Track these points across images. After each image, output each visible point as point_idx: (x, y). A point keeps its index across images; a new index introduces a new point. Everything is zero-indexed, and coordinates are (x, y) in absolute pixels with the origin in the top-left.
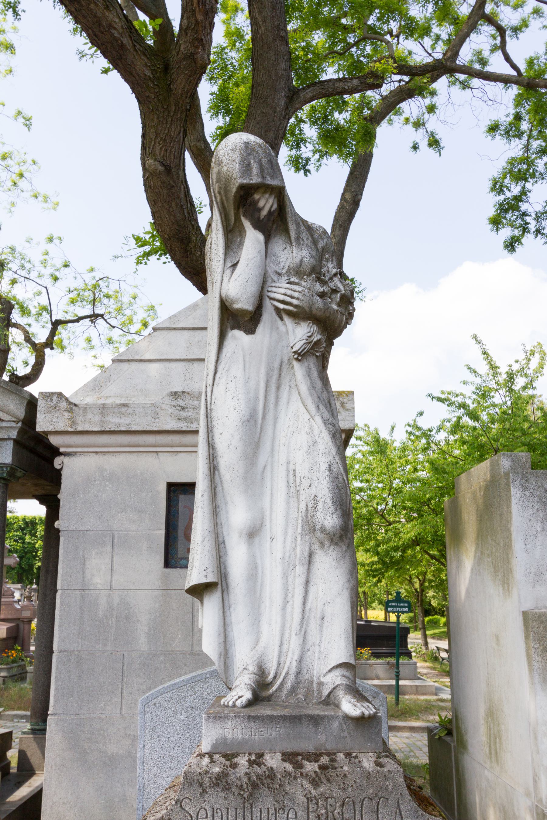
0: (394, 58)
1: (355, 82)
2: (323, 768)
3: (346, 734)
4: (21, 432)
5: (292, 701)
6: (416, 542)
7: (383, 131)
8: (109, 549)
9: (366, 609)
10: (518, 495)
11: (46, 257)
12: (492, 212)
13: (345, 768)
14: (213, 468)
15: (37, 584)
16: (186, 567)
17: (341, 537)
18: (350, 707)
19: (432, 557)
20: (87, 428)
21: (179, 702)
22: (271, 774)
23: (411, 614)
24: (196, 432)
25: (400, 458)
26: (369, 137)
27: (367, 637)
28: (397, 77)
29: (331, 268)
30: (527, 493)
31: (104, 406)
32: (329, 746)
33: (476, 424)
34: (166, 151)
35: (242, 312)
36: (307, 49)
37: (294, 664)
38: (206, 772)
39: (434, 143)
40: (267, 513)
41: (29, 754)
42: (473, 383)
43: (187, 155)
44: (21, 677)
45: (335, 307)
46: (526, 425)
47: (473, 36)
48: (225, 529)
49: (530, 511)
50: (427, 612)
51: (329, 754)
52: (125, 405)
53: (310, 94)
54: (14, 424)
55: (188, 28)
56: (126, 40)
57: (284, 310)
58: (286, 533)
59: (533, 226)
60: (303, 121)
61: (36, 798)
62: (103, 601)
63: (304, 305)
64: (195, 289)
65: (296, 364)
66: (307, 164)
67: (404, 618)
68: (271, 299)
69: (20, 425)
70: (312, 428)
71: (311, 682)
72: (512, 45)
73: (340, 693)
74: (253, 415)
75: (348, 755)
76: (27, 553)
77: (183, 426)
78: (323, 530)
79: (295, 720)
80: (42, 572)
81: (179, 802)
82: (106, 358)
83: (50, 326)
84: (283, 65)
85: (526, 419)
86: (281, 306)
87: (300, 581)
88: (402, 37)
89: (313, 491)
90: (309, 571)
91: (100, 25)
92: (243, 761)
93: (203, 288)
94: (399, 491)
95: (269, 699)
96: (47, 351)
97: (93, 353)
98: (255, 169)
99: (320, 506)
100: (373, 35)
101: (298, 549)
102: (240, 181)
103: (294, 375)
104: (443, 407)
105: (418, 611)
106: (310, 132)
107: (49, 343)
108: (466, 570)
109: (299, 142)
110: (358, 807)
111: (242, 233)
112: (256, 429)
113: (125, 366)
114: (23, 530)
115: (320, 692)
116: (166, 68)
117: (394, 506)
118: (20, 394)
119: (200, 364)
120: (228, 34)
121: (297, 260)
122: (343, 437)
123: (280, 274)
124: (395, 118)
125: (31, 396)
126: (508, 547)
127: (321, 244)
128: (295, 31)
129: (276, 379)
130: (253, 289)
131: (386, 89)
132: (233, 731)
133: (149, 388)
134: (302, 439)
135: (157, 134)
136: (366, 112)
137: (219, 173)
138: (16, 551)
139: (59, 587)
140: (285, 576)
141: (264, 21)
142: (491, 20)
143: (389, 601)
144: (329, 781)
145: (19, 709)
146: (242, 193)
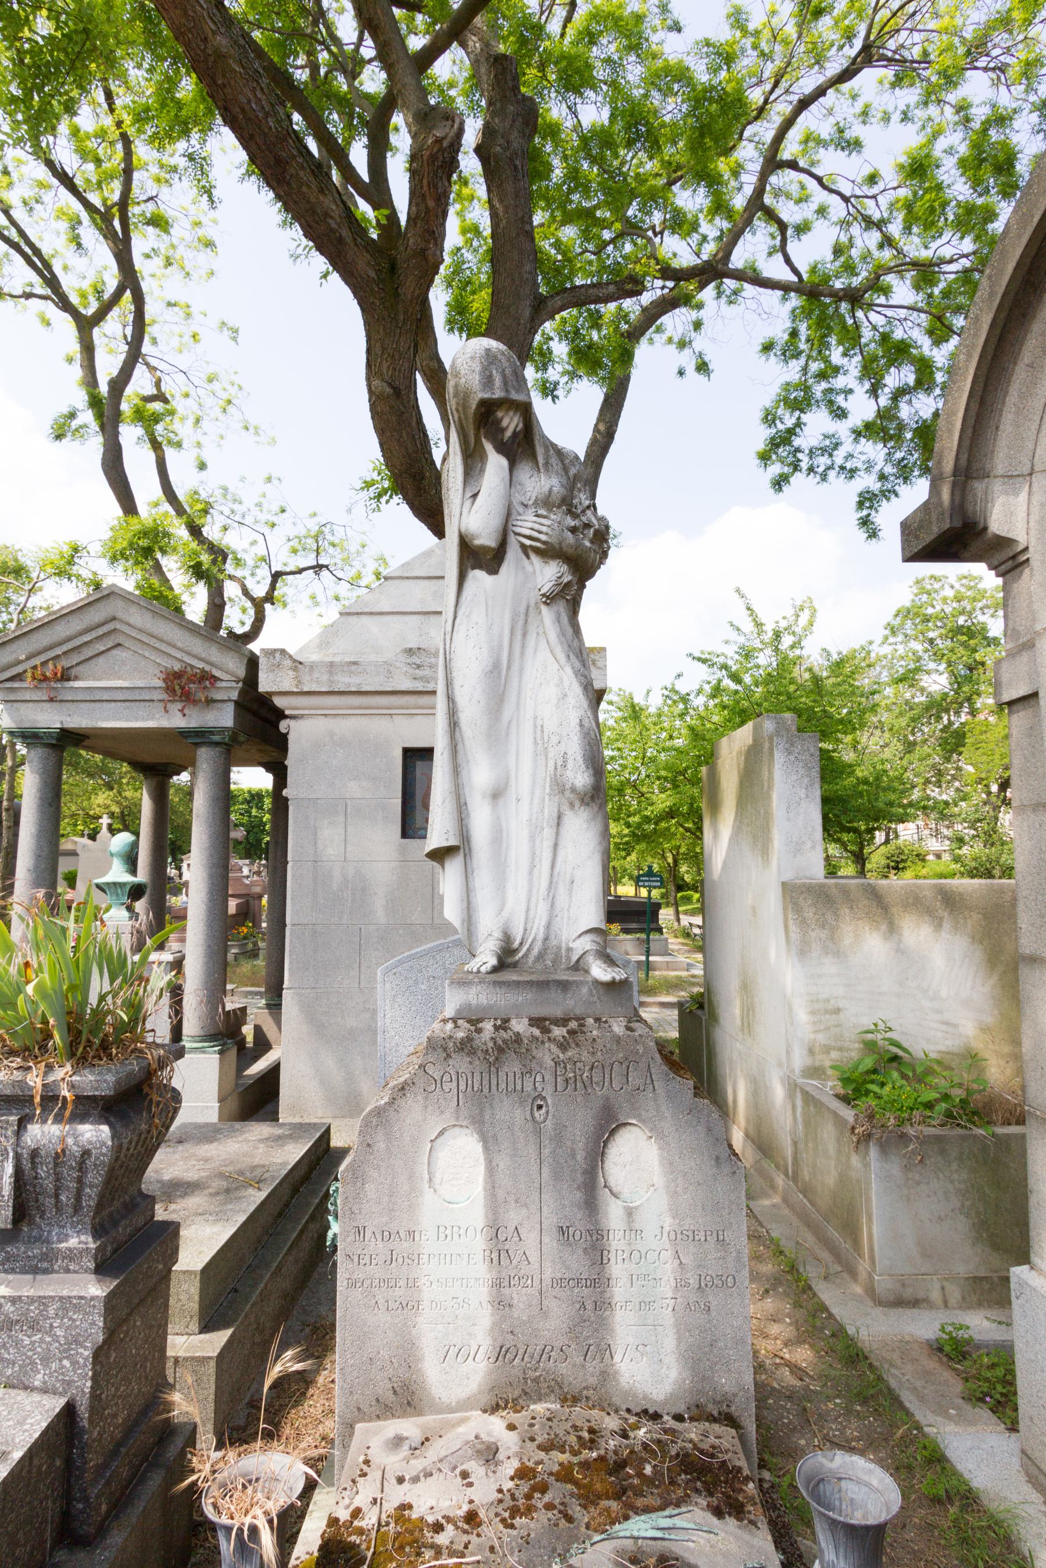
0: (656, 259)
1: (612, 288)
2: (572, 1032)
3: (595, 999)
4: (242, 693)
5: (539, 967)
6: (671, 813)
7: (642, 352)
8: (342, 818)
9: (615, 885)
10: (782, 760)
11: (262, 500)
12: (761, 446)
13: (595, 1033)
14: (453, 725)
15: (267, 859)
16: (425, 837)
17: (592, 797)
18: (600, 972)
19: (687, 830)
20: (314, 688)
21: (420, 971)
22: (518, 1038)
23: (663, 890)
24: (434, 693)
25: (655, 724)
26: (626, 357)
27: (620, 913)
28: (659, 283)
29: (583, 499)
30: (792, 758)
31: (332, 664)
32: (578, 1012)
33: (739, 687)
34: (394, 369)
35: (484, 549)
36: (557, 245)
37: (542, 930)
38: (451, 1037)
39: (703, 367)
40: (513, 773)
41: (265, 1029)
42: (735, 643)
43: (418, 377)
44: (254, 954)
45: (588, 544)
46: (792, 688)
47: (747, 235)
48: (467, 790)
49: (794, 777)
50: (680, 888)
51: (577, 1019)
52: (355, 663)
53: (559, 303)
54: (234, 684)
55: (417, 217)
56: (345, 233)
57: (531, 547)
58: (533, 793)
59: (804, 465)
60: (552, 339)
61: (274, 1072)
62: (337, 874)
63: (553, 540)
64: (429, 533)
65: (544, 609)
66: (555, 389)
67: (656, 894)
68: (516, 534)
69: (240, 685)
70: (561, 680)
71: (559, 948)
72: (793, 247)
73: (590, 959)
74: (496, 666)
75: (598, 1020)
76: (254, 828)
77: (419, 686)
78: (573, 790)
79: (543, 985)
80: (271, 847)
81: (422, 1067)
82: (332, 614)
83: (269, 580)
84: (528, 267)
85: (792, 681)
86: (528, 542)
87: (548, 844)
88: (666, 233)
89: (562, 748)
90: (557, 834)
91: (314, 212)
92: (488, 1026)
93: (439, 531)
94: (653, 760)
95: (515, 965)
96: (268, 606)
97: (318, 610)
98: (498, 381)
99: (570, 764)
100: (632, 229)
101: (546, 811)
102: (481, 395)
103: (542, 621)
104: (704, 667)
105: (671, 887)
106: (560, 349)
107: (269, 598)
108: (720, 840)
109: (545, 359)
110: (607, 1071)
111: (483, 457)
112: (499, 680)
113: (354, 619)
114: (248, 802)
115: (568, 958)
116: (393, 268)
117: (648, 776)
118: (238, 651)
119: (437, 617)
120: (464, 231)
121: (546, 489)
122: (597, 696)
123: (526, 506)
124: (656, 337)
125: (252, 653)
126: (768, 817)
127: (573, 471)
128: (542, 225)
129: (521, 625)
130: (495, 523)
131: (646, 298)
132: (479, 996)
133: (383, 643)
134: (551, 692)
135: (384, 349)
136: (624, 327)
137: (456, 386)
138: (242, 825)
139: (289, 859)
140: (532, 838)
141: (506, 211)
142: (771, 215)
143: (639, 876)
144: (577, 1045)
145: (253, 985)
146: (483, 410)
